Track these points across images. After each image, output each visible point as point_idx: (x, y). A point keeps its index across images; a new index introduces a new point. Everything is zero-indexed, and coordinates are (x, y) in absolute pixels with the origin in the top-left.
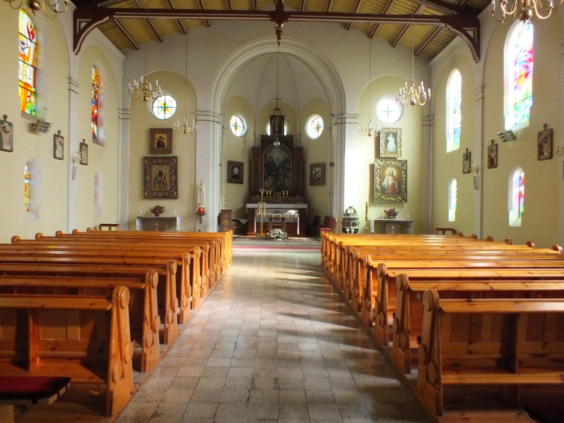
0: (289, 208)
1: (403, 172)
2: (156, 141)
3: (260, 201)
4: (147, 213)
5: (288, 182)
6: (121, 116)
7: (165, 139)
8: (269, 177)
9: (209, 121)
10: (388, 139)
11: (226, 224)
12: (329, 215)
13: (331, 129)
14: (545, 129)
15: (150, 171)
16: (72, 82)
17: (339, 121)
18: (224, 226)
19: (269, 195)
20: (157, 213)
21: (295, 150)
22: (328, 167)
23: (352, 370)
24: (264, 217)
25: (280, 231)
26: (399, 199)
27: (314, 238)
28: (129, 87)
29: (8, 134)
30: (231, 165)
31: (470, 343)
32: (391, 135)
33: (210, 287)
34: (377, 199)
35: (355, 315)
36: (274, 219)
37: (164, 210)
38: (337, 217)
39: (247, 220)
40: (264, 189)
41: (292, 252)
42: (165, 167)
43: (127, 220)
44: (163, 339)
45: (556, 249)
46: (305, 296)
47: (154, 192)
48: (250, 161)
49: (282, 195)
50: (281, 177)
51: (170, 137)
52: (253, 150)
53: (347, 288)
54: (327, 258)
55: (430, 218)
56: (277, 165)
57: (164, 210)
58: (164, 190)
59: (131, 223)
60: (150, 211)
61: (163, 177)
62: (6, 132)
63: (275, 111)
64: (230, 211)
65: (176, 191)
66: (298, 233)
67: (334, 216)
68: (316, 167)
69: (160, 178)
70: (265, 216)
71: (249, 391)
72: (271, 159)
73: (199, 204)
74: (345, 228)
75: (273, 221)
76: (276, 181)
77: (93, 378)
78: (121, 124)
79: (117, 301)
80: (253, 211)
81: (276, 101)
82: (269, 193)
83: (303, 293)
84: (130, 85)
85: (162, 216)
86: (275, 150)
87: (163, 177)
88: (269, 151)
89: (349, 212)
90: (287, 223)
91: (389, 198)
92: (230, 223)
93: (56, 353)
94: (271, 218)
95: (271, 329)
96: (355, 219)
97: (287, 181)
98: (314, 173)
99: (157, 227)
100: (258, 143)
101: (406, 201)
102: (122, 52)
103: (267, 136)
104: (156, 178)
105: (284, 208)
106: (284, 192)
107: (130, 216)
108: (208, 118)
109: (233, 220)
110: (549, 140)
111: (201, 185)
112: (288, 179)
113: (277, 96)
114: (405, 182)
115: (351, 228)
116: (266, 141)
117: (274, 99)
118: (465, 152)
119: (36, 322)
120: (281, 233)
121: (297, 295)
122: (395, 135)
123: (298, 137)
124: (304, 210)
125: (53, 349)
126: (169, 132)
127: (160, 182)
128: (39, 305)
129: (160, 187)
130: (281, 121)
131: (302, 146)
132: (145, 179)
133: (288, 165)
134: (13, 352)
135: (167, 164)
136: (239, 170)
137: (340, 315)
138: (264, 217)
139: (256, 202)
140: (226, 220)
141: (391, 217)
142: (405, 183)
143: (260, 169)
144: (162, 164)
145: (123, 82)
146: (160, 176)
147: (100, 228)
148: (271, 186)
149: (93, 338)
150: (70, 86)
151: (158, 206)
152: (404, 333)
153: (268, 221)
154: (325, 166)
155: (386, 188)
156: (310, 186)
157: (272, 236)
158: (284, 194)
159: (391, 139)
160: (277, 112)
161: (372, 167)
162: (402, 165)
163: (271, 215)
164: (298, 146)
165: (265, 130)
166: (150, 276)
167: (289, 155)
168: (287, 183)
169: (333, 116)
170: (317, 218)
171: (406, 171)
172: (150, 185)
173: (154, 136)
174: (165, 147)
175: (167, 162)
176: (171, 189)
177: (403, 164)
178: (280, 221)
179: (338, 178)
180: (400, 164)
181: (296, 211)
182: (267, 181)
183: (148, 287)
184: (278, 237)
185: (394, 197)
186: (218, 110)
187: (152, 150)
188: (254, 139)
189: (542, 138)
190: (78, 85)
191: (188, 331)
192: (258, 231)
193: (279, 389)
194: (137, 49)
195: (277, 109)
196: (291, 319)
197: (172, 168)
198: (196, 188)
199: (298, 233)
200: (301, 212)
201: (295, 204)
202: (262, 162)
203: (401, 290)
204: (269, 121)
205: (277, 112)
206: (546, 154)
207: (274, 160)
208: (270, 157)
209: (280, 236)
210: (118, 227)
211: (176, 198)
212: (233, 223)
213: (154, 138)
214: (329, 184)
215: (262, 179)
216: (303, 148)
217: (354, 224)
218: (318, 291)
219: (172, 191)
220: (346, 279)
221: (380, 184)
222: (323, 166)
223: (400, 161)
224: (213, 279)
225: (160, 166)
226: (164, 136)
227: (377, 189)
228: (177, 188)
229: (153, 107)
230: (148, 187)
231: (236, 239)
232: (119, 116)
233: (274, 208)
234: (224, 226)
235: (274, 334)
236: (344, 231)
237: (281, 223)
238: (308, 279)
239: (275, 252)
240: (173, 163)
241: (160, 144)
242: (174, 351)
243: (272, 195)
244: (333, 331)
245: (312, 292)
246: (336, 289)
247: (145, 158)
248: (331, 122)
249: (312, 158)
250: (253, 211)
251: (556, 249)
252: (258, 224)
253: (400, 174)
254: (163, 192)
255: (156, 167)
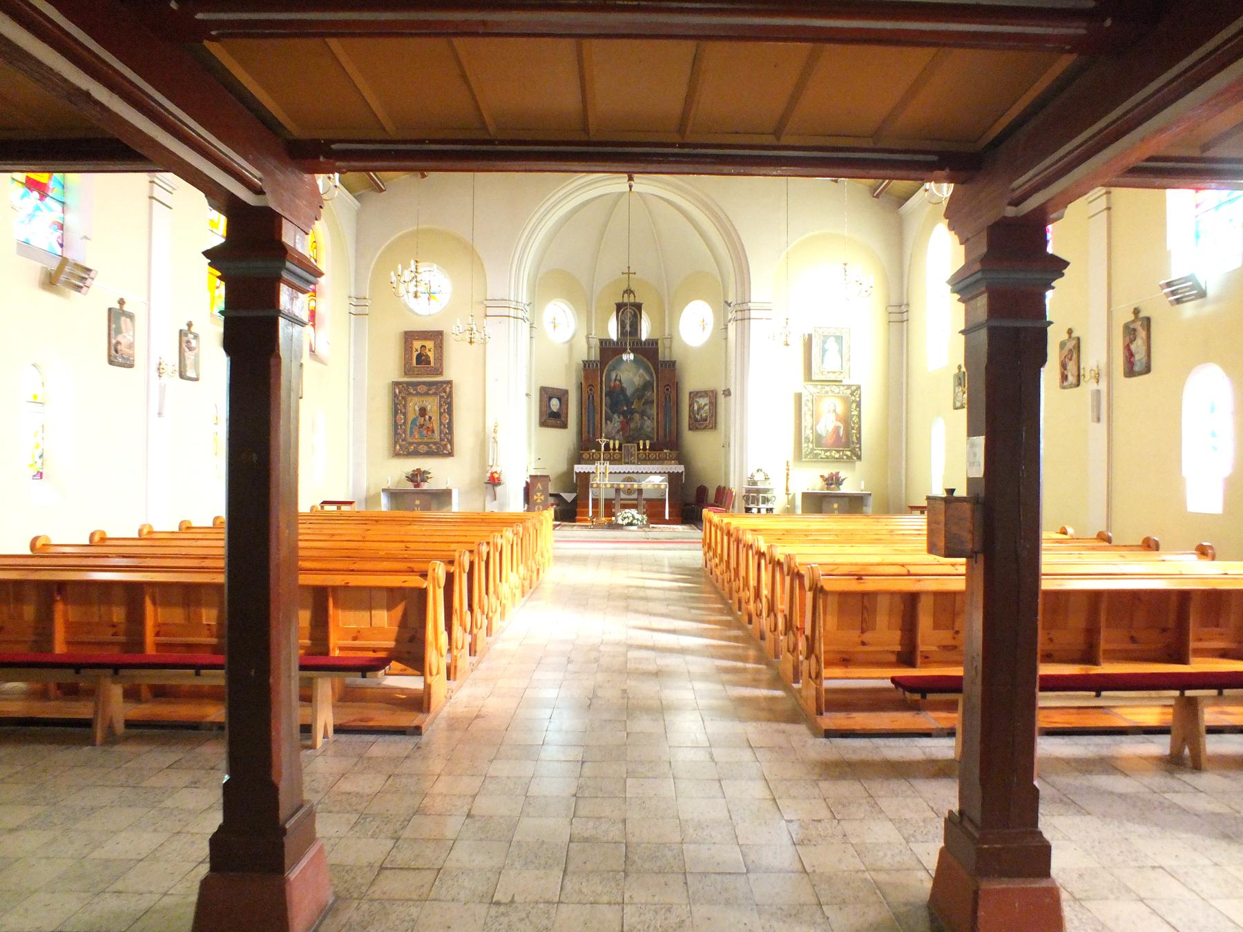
0: (651, 473)
1: (854, 405)
2: (415, 354)
3: (599, 459)
4: (399, 482)
5: (649, 425)
6: (353, 310)
7: (430, 350)
8: (616, 416)
9: (509, 316)
10: (826, 346)
11: (539, 501)
12: (723, 485)
13: (726, 328)
14: (1070, 337)
15: (405, 406)
16: (156, 180)
17: (739, 315)
18: (536, 504)
19: (614, 449)
20: (417, 482)
21: (662, 365)
22: (721, 399)
23: (723, 683)
24: (606, 488)
25: (634, 512)
26: (847, 455)
27: (695, 524)
28: (391, 277)
29: (194, 352)
30: (547, 394)
31: (863, 632)
32: (832, 339)
33: (523, 594)
34: (808, 455)
35: (787, 688)
36: (624, 493)
37: (429, 476)
38: (736, 486)
39: (574, 495)
40: (606, 438)
41: (655, 549)
42: (430, 399)
43: (363, 494)
44: (472, 651)
45: (1065, 533)
46: (670, 608)
47: (411, 444)
48: (580, 387)
49: (639, 449)
50: (637, 416)
51: (439, 347)
52: (585, 365)
53: (789, 654)
54: (711, 554)
55: (904, 491)
56: (629, 392)
57: (429, 476)
58: (430, 440)
59: (371, 499)
60: (404, 477)
61: (427, 417)
62: (190, 349)
63: (626, 295)
64: (547, 477)
65: (451, 442)
66: (667, 517)
67: (731, 486)
68: (701, 397)
69: (423, 419)
70: (609, 486)
71: (590, 699)
72: (618, 383)
73: (492, 466)
74: (751, 506)
75: (623, 496)
76: (627, 423)
77: (405, 670)
78: (352, 323)
79: (434, 578)
80: (585, 477)
81: (627, 276)
82: (614, 444)
83: (668, 605)
84: (392, 273)
85: (425, 486)
86: (623, 367)
87: (427, 417)
88: (614, 368)
89: (756, 479)
90: (647, 500)
91: (828, 454)
92: (546, 500)
93: (357, 643)
94: (618, 490)
95: (618, 644)
96: (766, 491)
97: (648, 423)
98: (696, 408)
99: (417, 506)
100: (595, 355)
101: (859, 458)
102: (355, 197)
103: (610, 341)
104: (415, 420)
105: (642, 473)
106: (641, 442)
107: (368, 490)
108: (505, 311)
109: (551, 495)
110: (1075, 356)
111: (495, 432)
112: (649, 419)
113: (629, 267)
114: (857, 423)
115: (761, 506)
116: (609, 351)
117: (623, 273)
118: (957, 371)
119: (336, 605)
120: (637, 516)
121: (661, 608)
122: (839, 339)
123: (667, 343)
124: (679, 475)
125: (355, 639)
126: (437, 337)
127: (422, 426)
128: (343, 583)
129: (422, 436)
130: (635, 314)
131: (673, 359)
132: (395, 421)
133: (648, 394)
134: (307, 642)
135: (435, 394)
136: (560, 403)
137: (721, 629)
138: (606, 488)
139: (591, 461)
140: (539, 494)
141: (833, 486)
142: (857, 426)
143: (597, 399)
144: (427, 394)
145: (357, 250)
146: (422, 416)
147: (322, 507)
148: (618, 432)
149: (403, 624)
150: (151, 189)
151: (418, 470)
152: (793, 632)
153: (612, 495)
154: (716, 394)
155: (824, 435)
156: (691, 432)
157: (620, 522)
158: (641, 447)
159: (832, 345)
160: (629, 297)
161: (799, 397)
162: (852, 394)
163: (619, 485)
164: (667, 359)
165: (605, 328)
166: (460, 557)
167: (651, 374)
168: (648, 427)
169: (729, 305)
170: (702, 491)
171: (859, 405)
172: (405, 432)
173: (412, 344)
174: (430, 364)
175: (434, 390)
176: (442, 440)
177: (854, 392)
178: (635, 496)
179: (738, 417)
180: (849, 391)
181: (663, 478)
182: (611, 422)
183: (458, 571)
184: (630, 524)
185: (838, 451)
186: (524, 298)
187: (408, 371)
188: (586, 346)
189: (1066, 351)
190: (174, 189)
191: (498, 646)
192: (596, 514)
193: (628, 698)
194: (381, 190)
195: (629, 291)
196: (649, 633)
197: (443, 400)
198: (485, 435)
199: (667, 517)
200: (673, 478)
201: (662, 464)
202: (601, 388)
203: (788, 575)
204: (615, 313)
205: (629, 297)
206: (1071, 379)
207: (624, 385)
208: (615, 380)
209: (635, 522)
210: (353, 505)
211: (450, 454)
212: (551, 500)
213: (411, 348)
214: (723, 427)
215: (601, 421)
216: (675, 362)
217: (766, 500)
218: (694, 602)
219: (444, 443)
220: (735, 581)
221: (812, 428)
222: (712, 396)
223: (849, 387)
224: (527, 583)
225: (422, 399)
226: (430, 344)
227: (807, 438)
228: (452, 438)
229: (429, 315)
230: (401, 435)
231: (558, 528)
232: (350, 309)
233: (624, 473)
234: (536, 504)
235: (622, 649)
236: (748, 510)
237: (636, 500)
238: (679, 587)
239: (626, 549)
240: (444, 392)
241: (422, 359)
242: (482, 666)
243: (620, 448)
244: (707, 646)
245: (684, 604)
246: (723, 600)
247: (396, 384)
248: (725, 316)
249: (692, 381)
250: (585, 477)
251: (1065, 533)
252: (596, 502)
253: (849, 410)
254: (427, 444)
255: (416, 399)
